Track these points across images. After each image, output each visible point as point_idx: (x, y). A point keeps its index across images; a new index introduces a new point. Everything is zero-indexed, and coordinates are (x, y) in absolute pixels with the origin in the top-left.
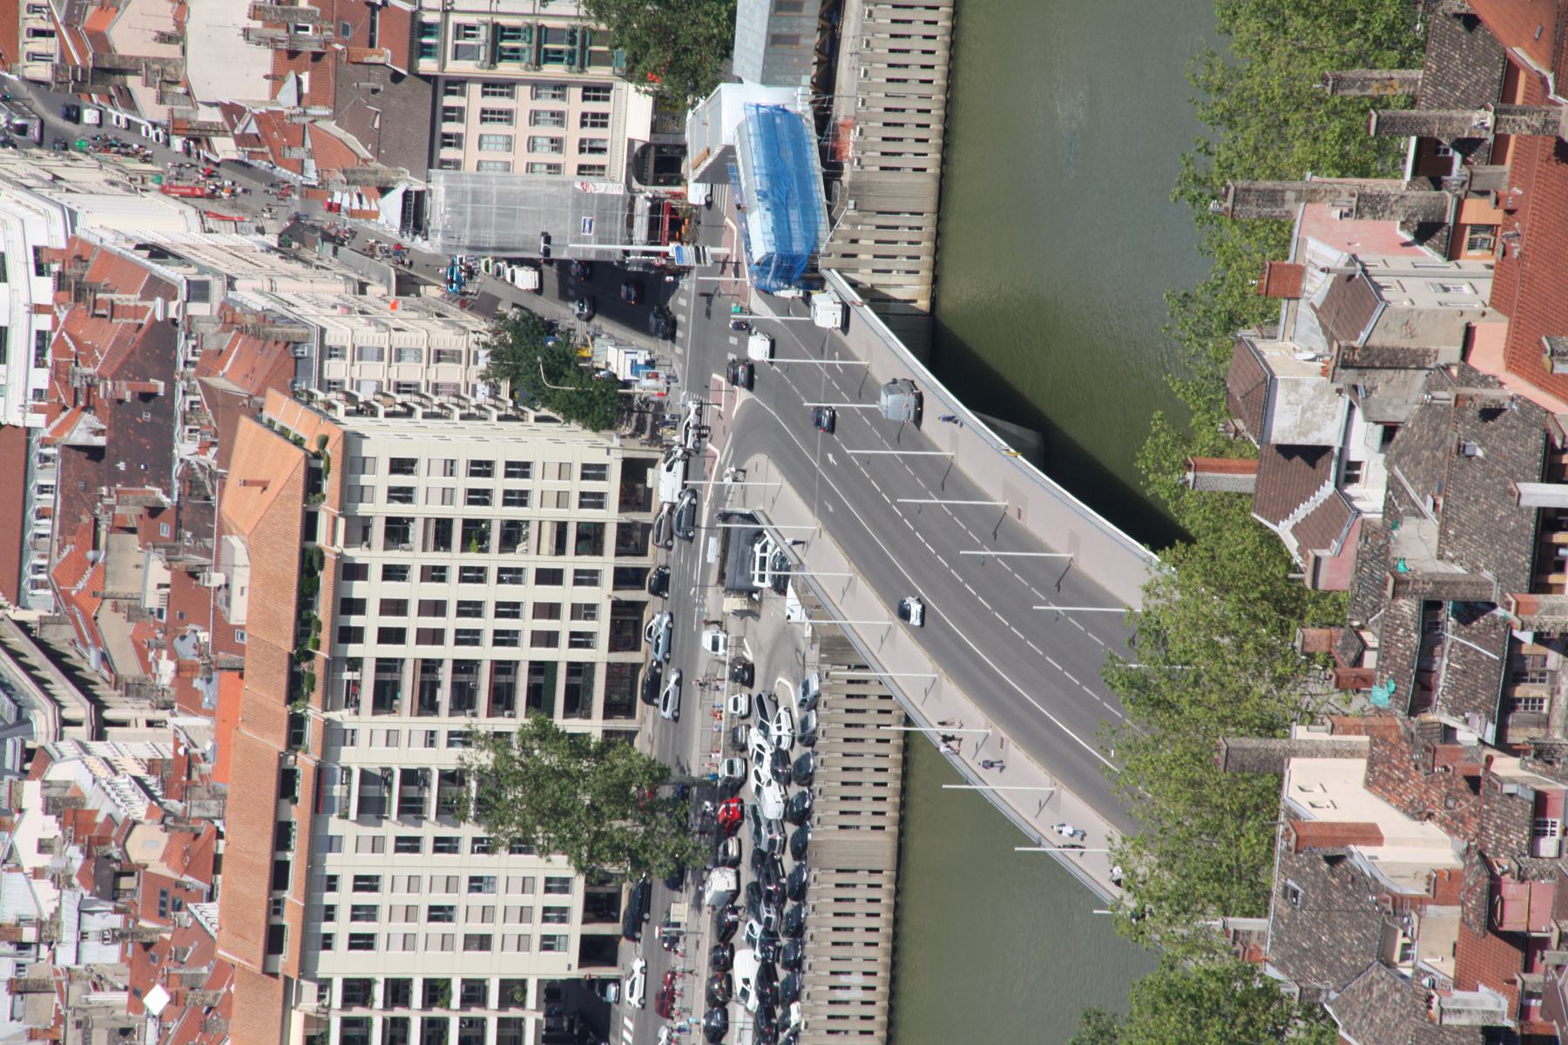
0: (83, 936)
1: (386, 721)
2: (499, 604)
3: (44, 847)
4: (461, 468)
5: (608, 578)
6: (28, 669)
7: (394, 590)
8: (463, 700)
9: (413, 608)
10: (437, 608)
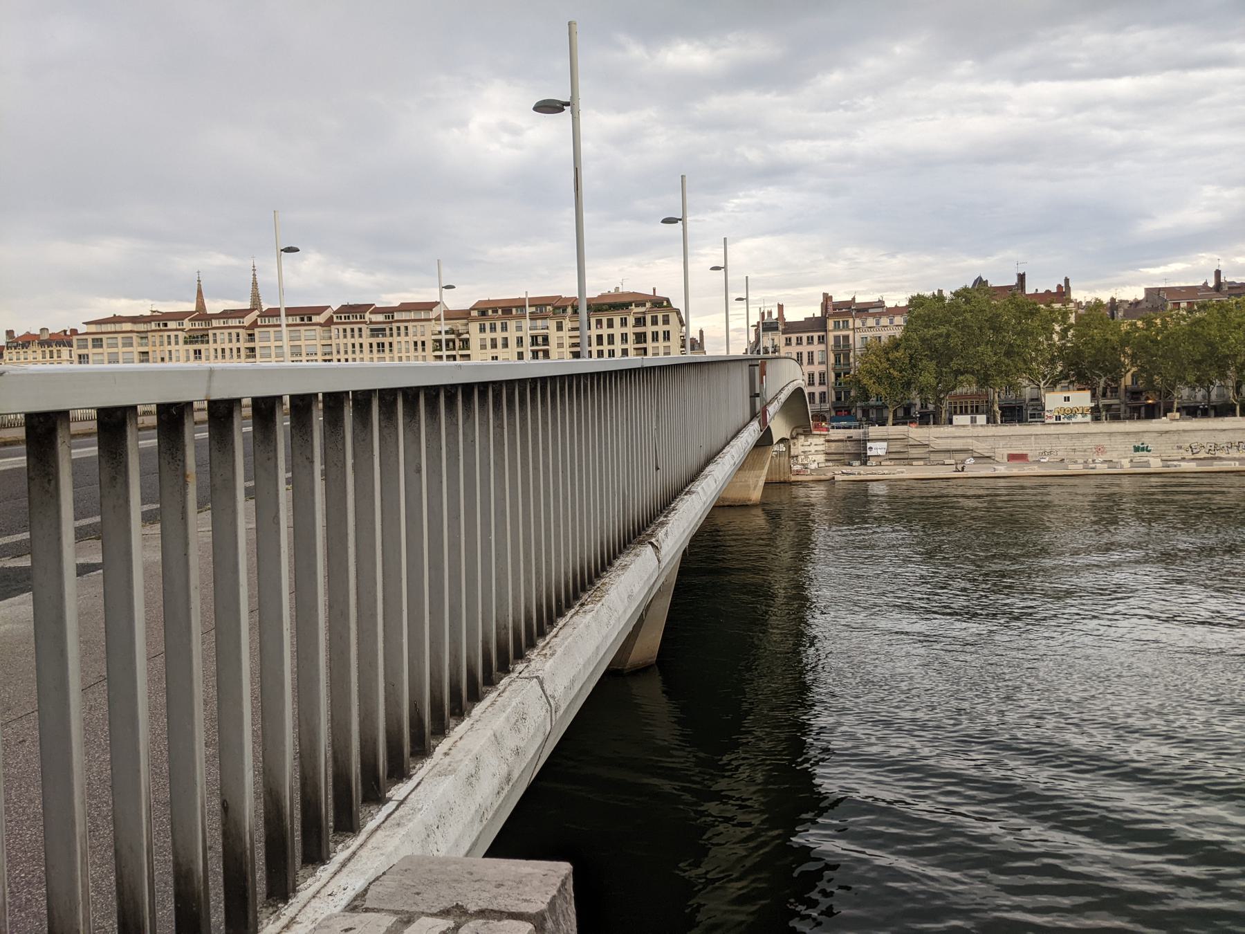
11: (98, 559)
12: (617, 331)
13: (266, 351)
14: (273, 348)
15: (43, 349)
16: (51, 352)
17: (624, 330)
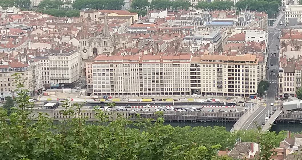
0: (195, 48)
1: (227, 71)
2: (240, 78)
3: (204, 44)
4: (254, 81)
5: (243, 93)
6: (218, 40)
7: (241, 71)
8: (229, 83)
9: (239, 73)
10: (239, 75)
11: (163, 60)
12: (241, 69)
13: (145, 70)
14: (147, 69)
15: (62, 56)
16: (64, 57)
17: (243, 69)
